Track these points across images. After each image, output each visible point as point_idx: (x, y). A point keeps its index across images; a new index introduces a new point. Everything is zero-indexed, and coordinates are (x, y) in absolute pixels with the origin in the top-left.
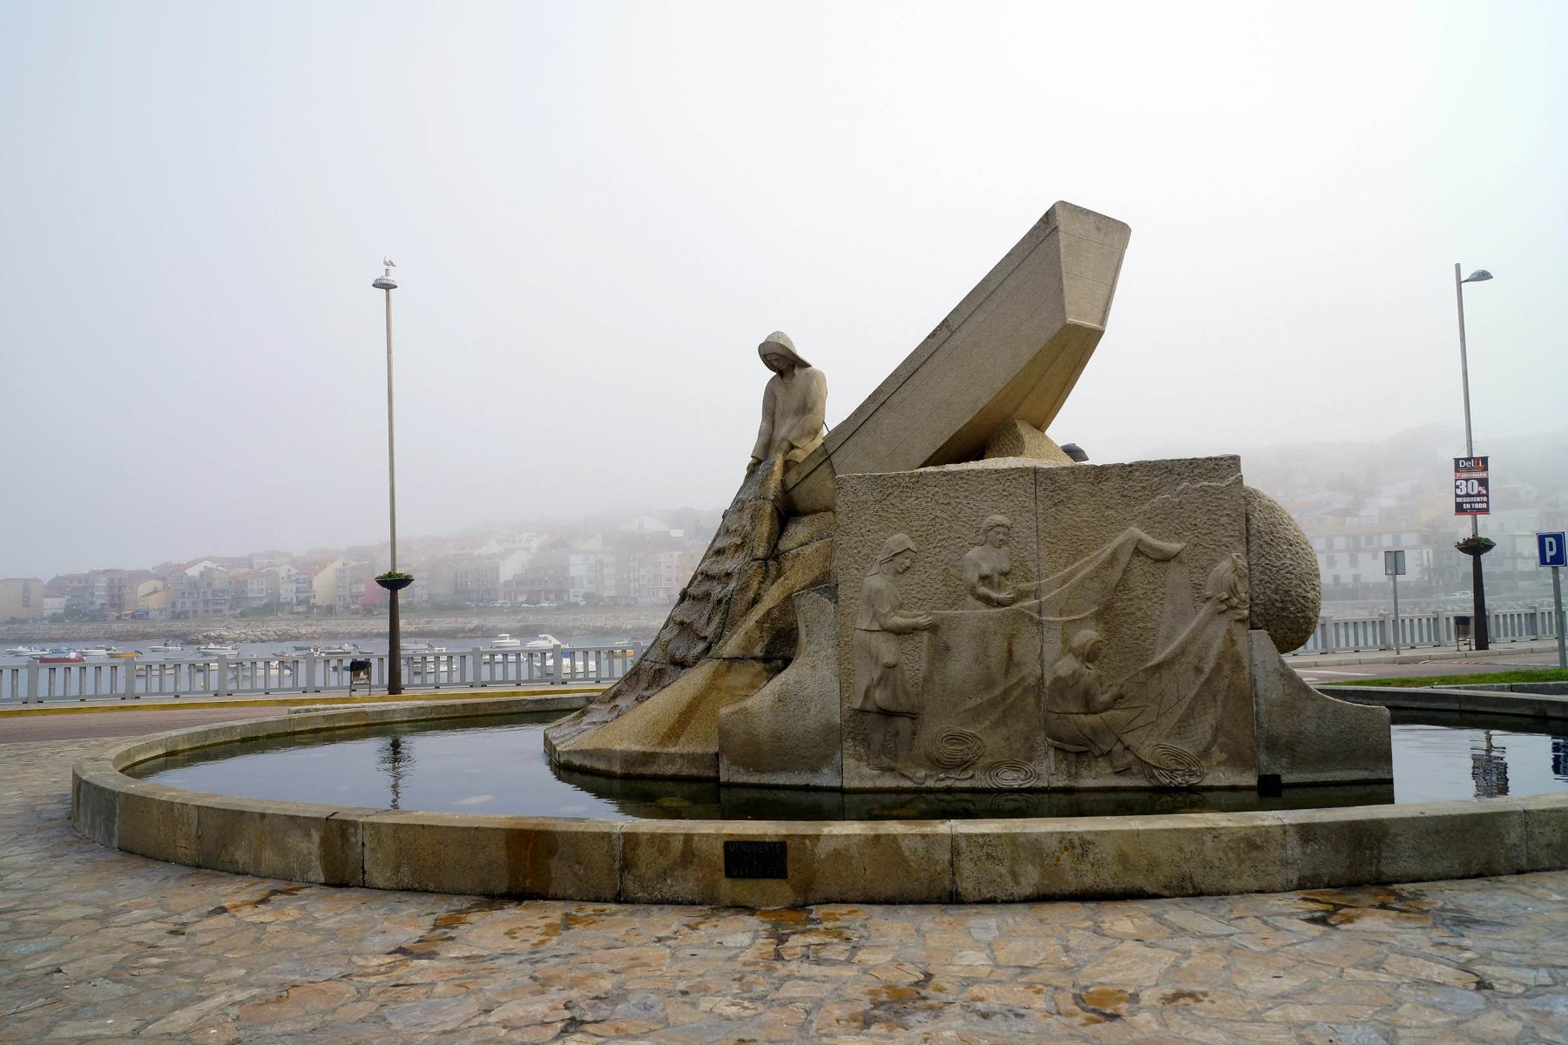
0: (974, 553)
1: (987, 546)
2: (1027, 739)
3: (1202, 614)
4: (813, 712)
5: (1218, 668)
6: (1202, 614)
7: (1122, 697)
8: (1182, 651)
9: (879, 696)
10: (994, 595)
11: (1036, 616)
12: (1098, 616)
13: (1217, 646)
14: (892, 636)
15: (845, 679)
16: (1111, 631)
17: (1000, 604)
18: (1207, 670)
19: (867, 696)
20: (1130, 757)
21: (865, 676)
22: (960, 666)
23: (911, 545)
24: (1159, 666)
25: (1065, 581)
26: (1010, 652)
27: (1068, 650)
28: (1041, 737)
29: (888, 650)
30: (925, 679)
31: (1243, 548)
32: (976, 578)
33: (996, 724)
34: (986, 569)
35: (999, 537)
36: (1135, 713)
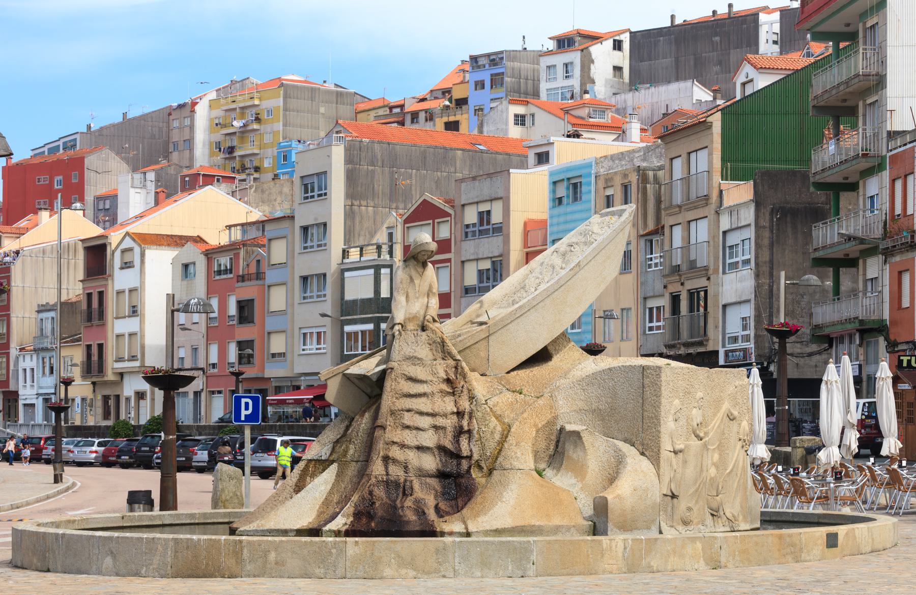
33: (697, 502)
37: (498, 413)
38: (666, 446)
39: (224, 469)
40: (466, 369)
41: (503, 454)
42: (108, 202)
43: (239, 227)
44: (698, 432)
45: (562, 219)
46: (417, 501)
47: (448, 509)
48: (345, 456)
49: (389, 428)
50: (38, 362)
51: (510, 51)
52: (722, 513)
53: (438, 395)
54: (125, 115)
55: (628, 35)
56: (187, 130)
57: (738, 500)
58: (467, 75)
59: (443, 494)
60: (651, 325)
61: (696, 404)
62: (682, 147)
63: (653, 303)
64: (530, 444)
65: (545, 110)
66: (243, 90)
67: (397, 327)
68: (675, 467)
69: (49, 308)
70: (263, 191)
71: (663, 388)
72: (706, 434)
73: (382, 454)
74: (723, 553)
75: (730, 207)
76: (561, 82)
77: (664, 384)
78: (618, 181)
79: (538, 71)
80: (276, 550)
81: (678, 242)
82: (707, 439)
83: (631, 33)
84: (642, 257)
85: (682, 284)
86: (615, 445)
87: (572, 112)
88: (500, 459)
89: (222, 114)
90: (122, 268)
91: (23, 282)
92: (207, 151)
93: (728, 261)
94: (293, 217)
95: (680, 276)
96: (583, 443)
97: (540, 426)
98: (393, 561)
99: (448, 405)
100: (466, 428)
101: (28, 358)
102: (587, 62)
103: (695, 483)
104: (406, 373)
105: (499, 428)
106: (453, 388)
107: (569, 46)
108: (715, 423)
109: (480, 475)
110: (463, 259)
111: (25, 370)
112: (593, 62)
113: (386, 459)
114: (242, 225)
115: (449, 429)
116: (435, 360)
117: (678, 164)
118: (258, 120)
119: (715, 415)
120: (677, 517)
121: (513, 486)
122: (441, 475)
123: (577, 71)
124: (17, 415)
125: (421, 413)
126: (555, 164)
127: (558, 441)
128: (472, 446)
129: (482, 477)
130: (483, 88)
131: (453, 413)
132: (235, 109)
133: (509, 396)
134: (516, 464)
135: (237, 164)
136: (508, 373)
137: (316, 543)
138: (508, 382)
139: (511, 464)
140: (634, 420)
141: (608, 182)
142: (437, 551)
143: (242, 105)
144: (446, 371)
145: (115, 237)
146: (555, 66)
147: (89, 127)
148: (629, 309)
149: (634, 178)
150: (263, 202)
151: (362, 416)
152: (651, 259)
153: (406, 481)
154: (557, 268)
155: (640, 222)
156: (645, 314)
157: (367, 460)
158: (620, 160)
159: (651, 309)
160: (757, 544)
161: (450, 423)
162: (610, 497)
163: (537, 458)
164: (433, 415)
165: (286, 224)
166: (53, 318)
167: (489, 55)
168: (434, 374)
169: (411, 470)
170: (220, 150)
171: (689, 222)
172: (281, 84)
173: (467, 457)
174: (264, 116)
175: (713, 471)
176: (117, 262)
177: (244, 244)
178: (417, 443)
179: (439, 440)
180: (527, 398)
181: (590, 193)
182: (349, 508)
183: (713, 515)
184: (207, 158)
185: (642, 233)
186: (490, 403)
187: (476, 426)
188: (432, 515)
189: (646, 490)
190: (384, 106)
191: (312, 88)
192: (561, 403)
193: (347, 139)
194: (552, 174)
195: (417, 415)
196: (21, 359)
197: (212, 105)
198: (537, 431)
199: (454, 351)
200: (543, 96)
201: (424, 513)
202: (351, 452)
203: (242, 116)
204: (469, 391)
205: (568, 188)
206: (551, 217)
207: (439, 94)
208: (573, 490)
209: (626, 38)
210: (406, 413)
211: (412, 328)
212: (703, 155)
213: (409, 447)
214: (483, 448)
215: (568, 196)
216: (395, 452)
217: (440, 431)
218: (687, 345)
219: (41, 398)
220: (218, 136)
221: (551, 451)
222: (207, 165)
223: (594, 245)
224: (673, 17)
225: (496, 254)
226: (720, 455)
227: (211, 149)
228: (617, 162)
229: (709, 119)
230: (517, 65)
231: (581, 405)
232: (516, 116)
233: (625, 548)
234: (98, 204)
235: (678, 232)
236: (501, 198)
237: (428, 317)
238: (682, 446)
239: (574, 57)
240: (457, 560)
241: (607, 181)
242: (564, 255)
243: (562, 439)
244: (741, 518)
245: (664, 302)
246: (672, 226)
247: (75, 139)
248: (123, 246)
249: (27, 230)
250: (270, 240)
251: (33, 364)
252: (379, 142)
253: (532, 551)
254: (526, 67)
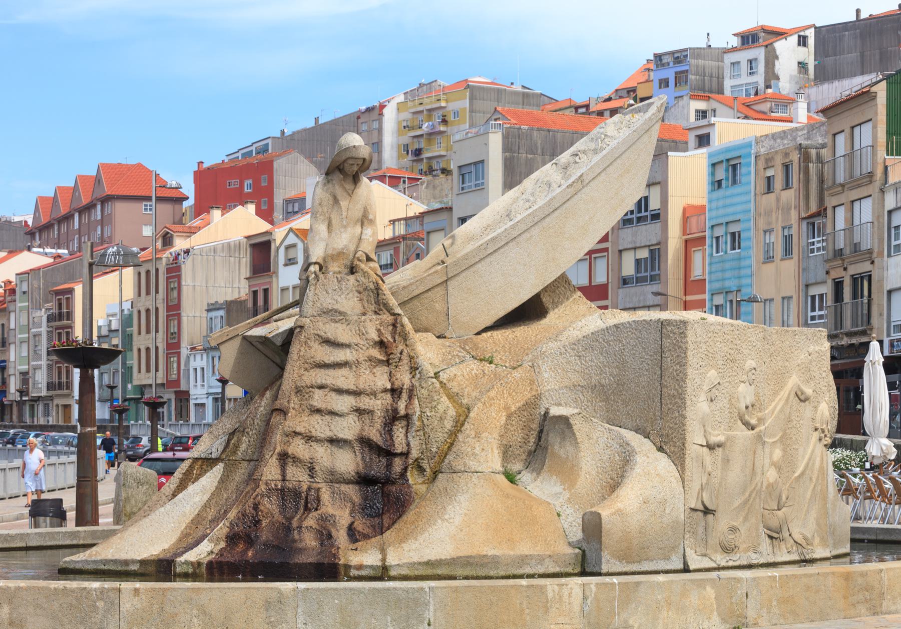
4: (667, 511)
24: (799, 476)
33: (746, 519)
37: (455, 390)
38: (695, 437)
39: (129, 471)
40: (409, 327)
41: (454, 449)
42: (296, 205)
43: (402, 222)
44: (747, 417)
45: (721, 203)
46: (324, 519)
47: (367, 531)
48: (235, 452)
49: (292, 413)
50: (208, 362)
51: (694, 49)
52: (786, 534)
53: (365, 365)
54: (316, 120)
55: (813, 30)
56: (375, 133)
57: (813, 515)
58: (652, 74)
59: (363, 508)
60: (813, 314)
61: (744, 378)
62: (845, 121)
63: (815, 291)
64: (496, 435)
65: (726, 105)
66: (431, 92)
67: (312, 268)
68: (709, 468)
69: (218, 306)
70: (434, 187)
71: (689, 353)
72: (761, 420)
73: (278, 450)
74: (751, 603)
75: (895, 183)
76: (745, 79)
77: (691, 346)
78: (779, 161)
79: (723, 68)
80: (10, 602)
81: (841, 224)
82: (762, 428)
83: (816, 28)
84: (804, 242)
85: (845, 269)
86: (621, 437)
87: (754, 107)
88: (450, 457)
89: (410, 116)
90: (286, 265)
91: (194, 281)
92: (395, 154)
93: (894, 243)
94: (451, 209)
95: (843, 260)
96: (574, 434)
97: (513, 409)
98: (195, 620)
99: (381, 379)
100: (402, 412)
101: (198, 357)
102: (771, 58)
103: (744, 492)
104: (322, 334)
105: (452, 412)
106: (388, 355)
107: (753, 42)
108: (775, 407)
109: (420, 480)
110: (621, 248)
111: (196, 369)
112: (777, 58)
113: (284, 458)
114: (406, 219)
115: (378, 413)
116: (364, 314)
117: (841, 140)
118: (444, 121)
119: (775, 393)
120: (713, 541)
121: (462, 498)
122: (364, 480)
123: (761, 68)
124: (188, 415)
125: (339, 391)
126: (716, 144)
127: (541, 431)
128: (410, 438)
129: (424, 483)
130: (667, 86)
131: (385, 391)
132: (422, 112)
133: (474, 366)
134: (473, 465)
135: (424, 166)
136: (478, 333)
137: (72, 591)
138: (476, 347)
139: (465, 465)
140: (648, 397)
141: (769, 162)
142: (268, 605)
143: (429, 107)
144: (379, 330)
145: (279, 234)
146: (739, 63)
147: (283, 132)
148: (790, 298)
149: (795, 157)
150: (434, 198)
151: (263, 395)
152: (813, 243)
153: (309, 489)
154: (555, 186)
155: (801, 204)
156: (806, 303)
157: (256, 460)
158: (782, 138)
159: (813, 297)
160: (808, 588)
161: (379, 404)
162: (605, 513)
163: (506, 453)
164: (356, 393)
165: (444, 216)
166: (222, 317)
167: (673, 53)
168: (361, 334)
169: (319, 473)
170: (408, 153)
171: (853, 202)
172: (467, 85)
173: (402, 454)
174: (451, 118)
175: (772, 475)
176: (282, 259)
177: (404, 238)
178: (329, 434)
179: (363, 430)
180: (500, 369)
181: (750, 176)
182: (222, 529)
183: (771, 537)
184: (395, 160)
185: (803, 215)
186: (443, 376)
187: (418, 410)
188: (341, 537)
189: (663, 502)
190: (570, 107)
191: (498, 89)
192: (546, 375)
193: (505, 126)
194: (710, 156)
195: (334, 394)
196: (192, 358)
197: (400, 107)
198: (509, 417)
199: (393, 302)
200: (728, 92)
201: (330, 536)
202: (243, 447)
203: (429, 118)
204: (411, 358)
205: (727, 170)
206: (710, 201)
207: (624, 93)
208: (555, 502)
209: (810, 34)
210: (317, 390)
211: (337, 269)
212: (867, 128)
213: (318, 440)
214: (427, 440)
215: (727, 179)
216: (298, 448)
217: (366, 416)
218: (850, 334)
219: (211, 398)
220: (406, 139)
221: (531, 445)
222: (395, 167)
223: (604, 152)
224: (858, 11)
225: (654, 242)
226: (784, 451)
227: (399, 151)
228: (779, 141)
229: (873, 89)
230: (701, 62)
231: (575, 378)
232: (697, 111)
233: (585, 598)
234: (287, 207)
235: (841, 213)
236: (659, 183)
237: (359, 254)
238: (721, 439)
239: (759, 53)
240: (301, 619)
241: (767, 160)
242: (565, 168)
243: (546, 428)
244: (817, 540)
245: (826, 289)
246: (834, 207)
247: (267, 144)
248: (287, 243)
249: (199, 228)
250: (428, 233)
251: (204, 363)
252: (538, 130)
253: (427, 604)
254: (710, 64)
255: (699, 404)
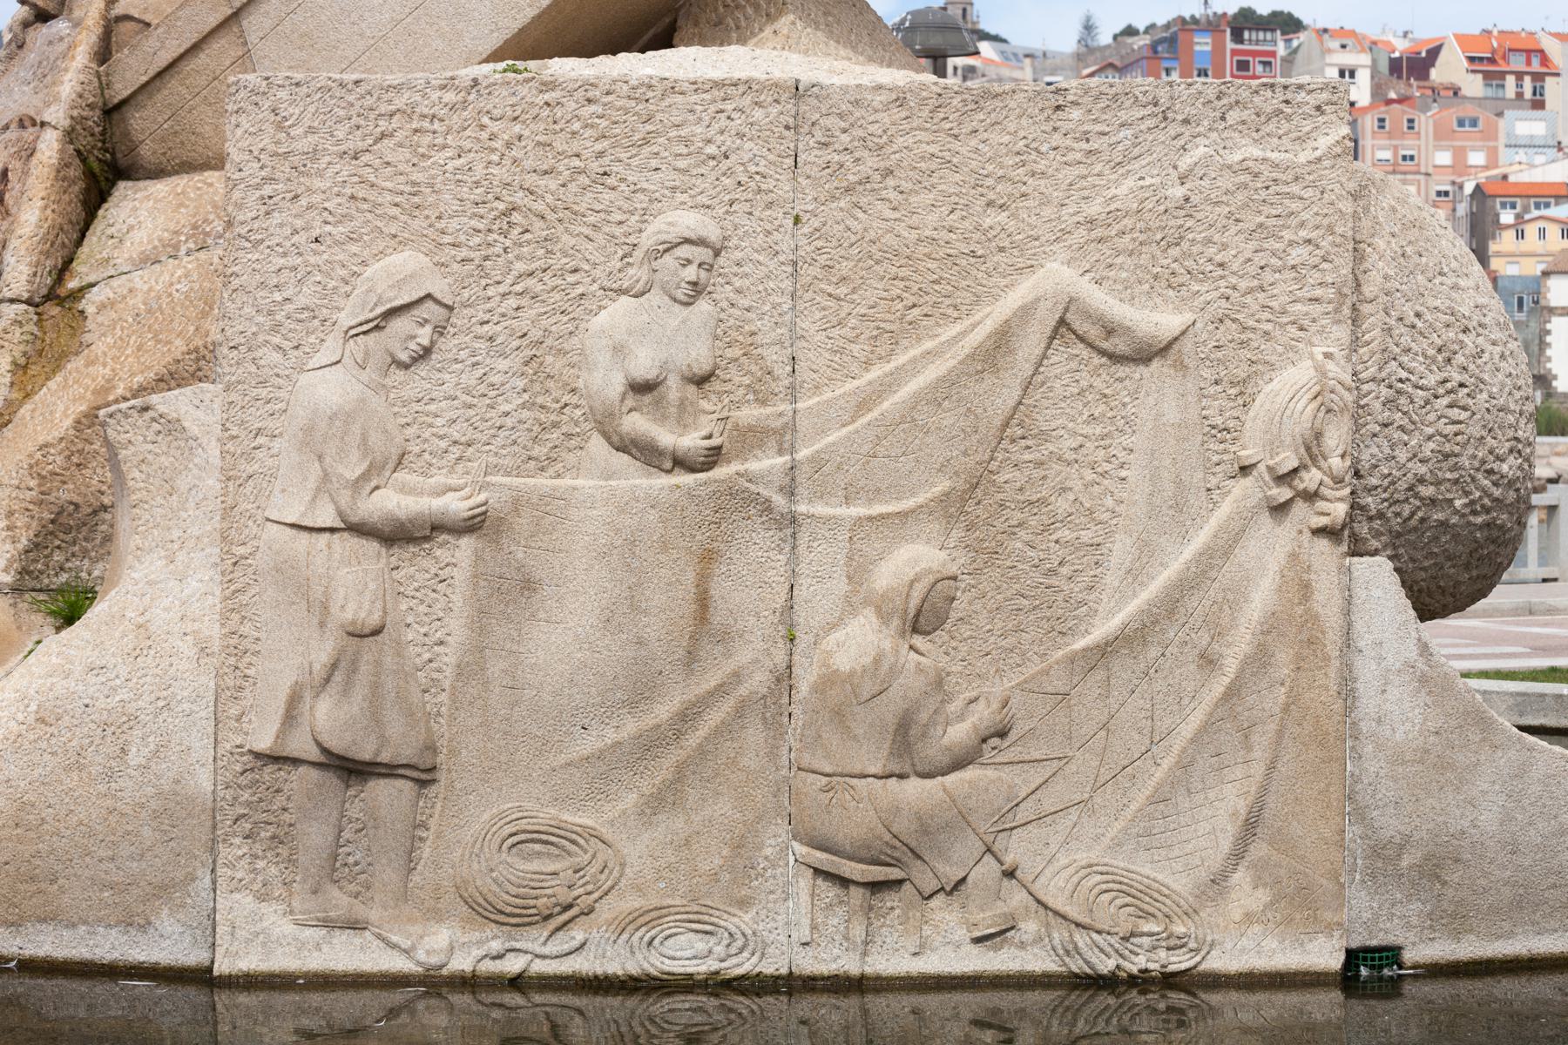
0: (617, 315)
1: (655, 298)
2: (738, 847)
3: (1225, 508)
4: (135, 757)
5: (1260, 658)
6: (1225, 508)
7: (1002, 734)
8: (1171, 604)
9: (331, 721)
10: (666, 438)
11: (779, 500)
12: (955, 507)
13: (1261, 598)
14: (373, 546)
15: (235, 659)
16: (986, 554)
17: (681, 463)
18: (1231, 666)
19: (290, 717)
20: (1017, 898)
21: (290, 653)
22: (566, 638)
23: (439, 286)
24: (1104, 651)
25: (863, 406)
26: (703, 602)
27: (857, 597)
28: (775, 839)
29: (355, 579)
30: (461, 671)
31: (1342, 333)
32: (617, 384)
33: (658, 803)
34: (643, 365)
35: (701, 271)
36: (1036, 776)
136: (1555, 580)
189: (119, 726)
255: (304, 379)
